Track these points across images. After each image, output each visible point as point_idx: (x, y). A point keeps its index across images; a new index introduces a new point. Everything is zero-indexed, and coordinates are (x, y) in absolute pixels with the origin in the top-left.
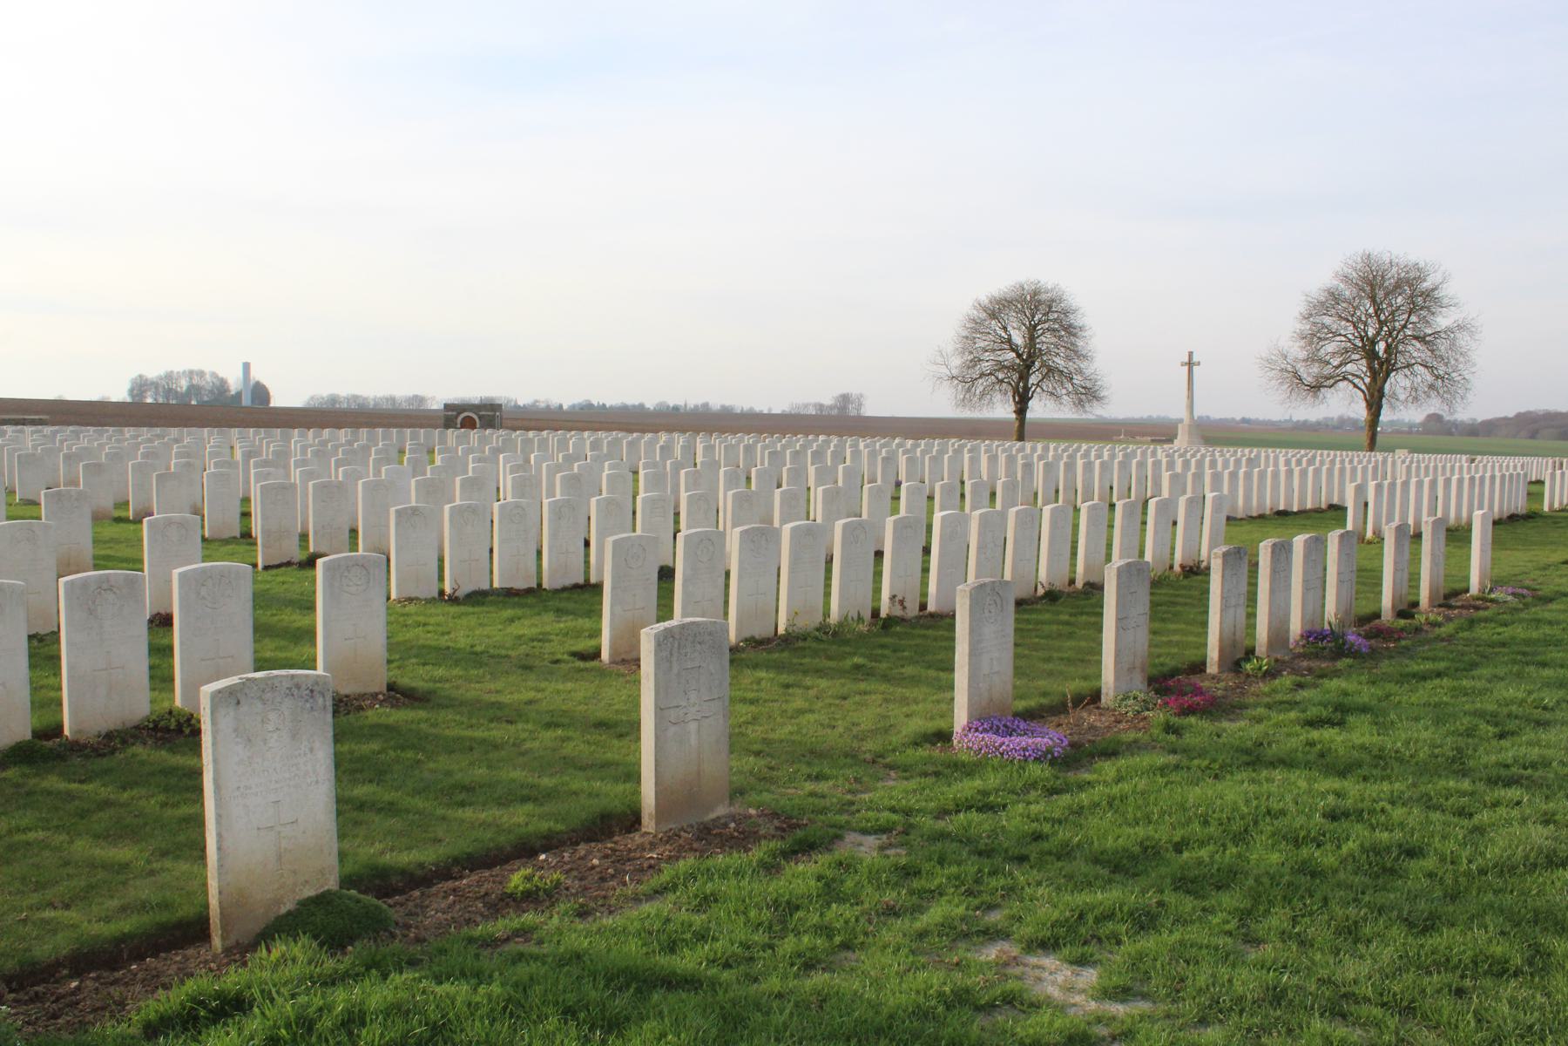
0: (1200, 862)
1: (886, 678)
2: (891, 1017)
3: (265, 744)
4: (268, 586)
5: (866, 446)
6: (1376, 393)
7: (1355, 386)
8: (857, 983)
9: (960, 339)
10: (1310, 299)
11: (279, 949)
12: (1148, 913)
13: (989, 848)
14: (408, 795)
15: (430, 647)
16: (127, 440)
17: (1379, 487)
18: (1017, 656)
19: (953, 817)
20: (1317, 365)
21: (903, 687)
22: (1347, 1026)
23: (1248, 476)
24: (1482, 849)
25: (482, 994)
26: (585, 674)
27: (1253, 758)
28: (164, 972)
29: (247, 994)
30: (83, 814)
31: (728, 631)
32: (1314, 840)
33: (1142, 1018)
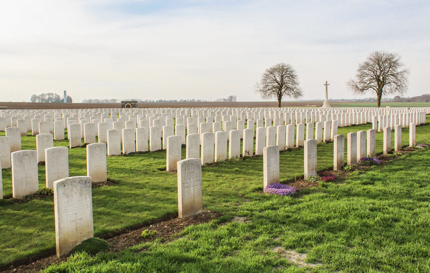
0: (334, 223)
1: (244, 173)
2: (249, 269)
3: (72, 197)
4: (73, 153)
5: (237, 110)
6: (380, 91)
7: (374, 89)
8: (239, 259)
9: (262, 80)
10: (360, 65)
11: (76, 255)
12: (320, 238)
13: (274, 220)
14: (113, 210)
15: (118, 168)
16: (31, 113)
17: (381, 117)
18: (280, 167)
19: (264, 212)
20: (363, 84)
21: (249, 176)
22: (380, 271)
23: (344, 115)
24: (417, 219)
25: (134, 266)
26: (162, 174)
27: (348, 194)
28: (42, 264)
29: (67, 269)
30: (18, 220)
31: (201, 162)
32: (367, 217)
33: (320, 268)
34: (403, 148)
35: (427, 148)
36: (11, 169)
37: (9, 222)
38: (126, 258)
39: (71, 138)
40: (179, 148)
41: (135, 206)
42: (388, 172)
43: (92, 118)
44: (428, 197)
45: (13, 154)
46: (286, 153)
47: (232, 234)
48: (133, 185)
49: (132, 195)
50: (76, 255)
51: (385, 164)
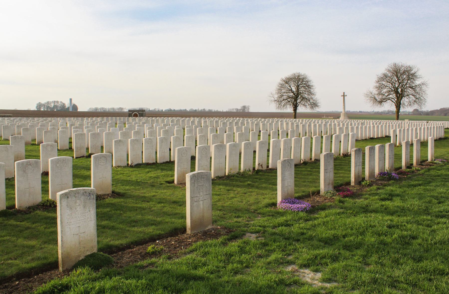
0: (351, 241)
1: (257, 188)
2: (261, 288)
3: (76, 209)
4: (77, 163)
6: (398, 104)
7: (392, 101)
12: (336, 256)
13: (288, 237)
14: (118, 224)
15: (124, 180)
16: (35, 121)
17: (400, 130)
18: (295, 181)
19: (278, 228)
20: (381, 95)
21: (262, 190)
22: (396, 290)
23: (361, 128)
24: (435, 237)
26: (170, 187)
27: (366, 210)
28: (44, 278)
29: (69, 284)
30: (21, 231)
32: (384, 234)
33: (335, 288)
34: (422, 162)
35: (445, 163)
36: (15, 179)
37: (12, 233)
38: (131, 275)
39: (75, 147)
40: (188, 160)
41: (140, 220)
42: (406, 188)
43: (98, 128)
44: (446, 213)
45: (17, 163)
46: (301, 166)
47: (243, 251)
48: (139, 198)
49: (138, 209)
50: (78, 270)
51: (404, 179)
